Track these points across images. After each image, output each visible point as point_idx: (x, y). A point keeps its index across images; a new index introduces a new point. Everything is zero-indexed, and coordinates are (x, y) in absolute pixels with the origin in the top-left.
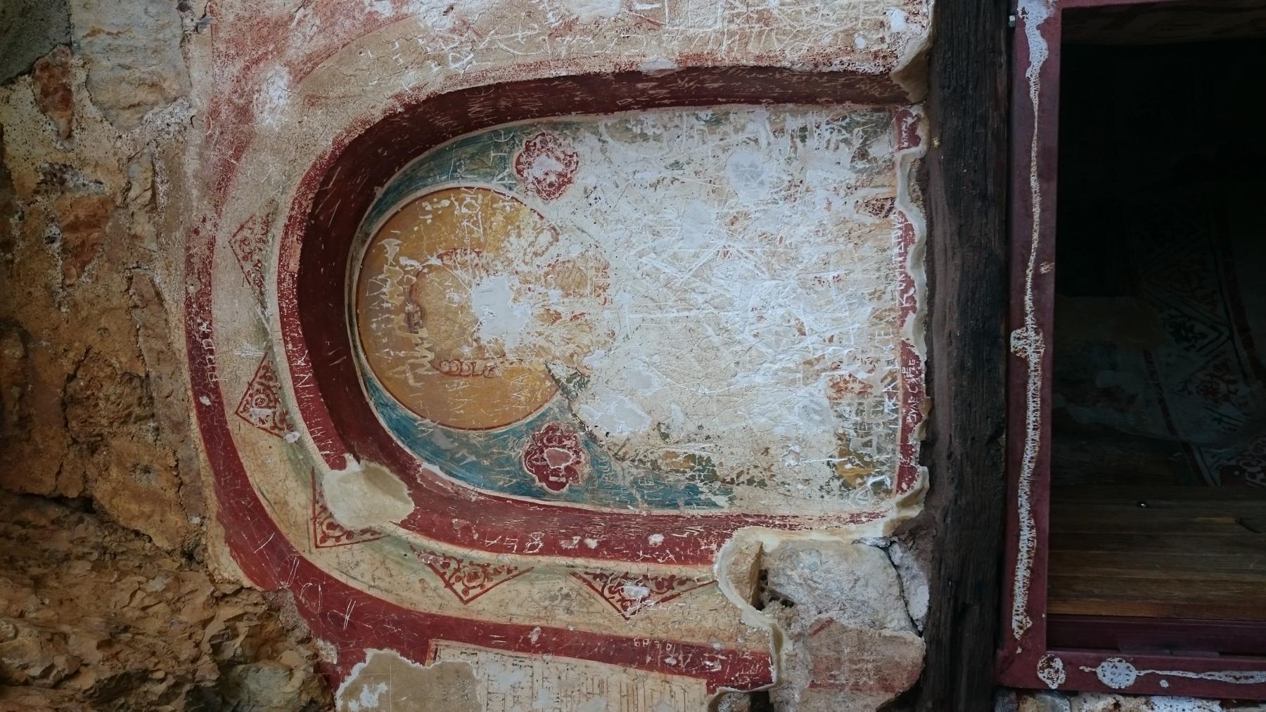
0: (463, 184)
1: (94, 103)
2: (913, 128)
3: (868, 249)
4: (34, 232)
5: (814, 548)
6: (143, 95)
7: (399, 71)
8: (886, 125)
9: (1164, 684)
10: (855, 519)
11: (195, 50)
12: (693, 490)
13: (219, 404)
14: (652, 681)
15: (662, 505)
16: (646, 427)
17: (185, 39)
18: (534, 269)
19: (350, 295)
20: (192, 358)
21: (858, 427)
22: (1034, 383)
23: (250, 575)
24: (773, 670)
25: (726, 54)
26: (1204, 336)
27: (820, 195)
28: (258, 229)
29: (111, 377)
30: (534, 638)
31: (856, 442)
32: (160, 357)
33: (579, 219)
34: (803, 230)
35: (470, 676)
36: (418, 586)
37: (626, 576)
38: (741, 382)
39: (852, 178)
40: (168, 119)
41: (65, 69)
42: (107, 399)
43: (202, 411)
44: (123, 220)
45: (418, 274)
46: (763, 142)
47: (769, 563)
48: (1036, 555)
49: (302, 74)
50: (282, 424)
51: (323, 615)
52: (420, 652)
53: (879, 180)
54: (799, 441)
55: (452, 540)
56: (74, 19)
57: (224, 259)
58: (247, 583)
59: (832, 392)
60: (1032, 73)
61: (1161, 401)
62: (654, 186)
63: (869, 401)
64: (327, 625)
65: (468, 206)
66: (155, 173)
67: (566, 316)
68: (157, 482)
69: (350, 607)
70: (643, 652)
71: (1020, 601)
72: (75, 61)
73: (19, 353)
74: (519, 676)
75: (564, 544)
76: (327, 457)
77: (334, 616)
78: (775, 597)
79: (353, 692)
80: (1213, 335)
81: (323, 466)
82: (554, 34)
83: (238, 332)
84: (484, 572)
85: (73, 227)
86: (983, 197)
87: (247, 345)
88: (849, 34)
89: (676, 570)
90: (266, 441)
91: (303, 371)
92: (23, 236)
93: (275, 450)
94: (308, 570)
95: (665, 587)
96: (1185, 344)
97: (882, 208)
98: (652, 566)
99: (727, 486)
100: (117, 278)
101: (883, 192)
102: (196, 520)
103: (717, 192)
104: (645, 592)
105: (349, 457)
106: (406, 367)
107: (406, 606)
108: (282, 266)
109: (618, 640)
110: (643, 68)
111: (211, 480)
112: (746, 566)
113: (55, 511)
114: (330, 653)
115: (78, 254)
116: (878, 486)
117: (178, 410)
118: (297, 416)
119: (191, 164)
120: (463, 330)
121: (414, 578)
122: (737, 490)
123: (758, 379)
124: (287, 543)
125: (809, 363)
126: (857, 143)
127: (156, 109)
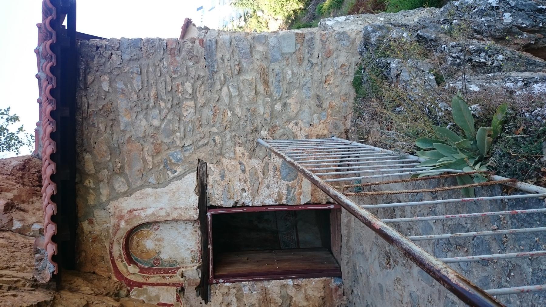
3: (194, 236)
5: (188, 270)
6: (104, 223)
7: (139, 221)
11: (111, 218)
12: (174, 265)
13: (114, 259)
14: (169, 288)
16: (168, 257)
17: (110, 217)
22: (211, 251)
27: (189, 230)
31: (194, 257)
32: (105, 254)
41: (92, 219)
43: (112, 260)
47: (183, 273)
48: (212, 269)
49: (126, 221)
50: (122, 261)
57: (115, 243)
60: (209, 220)
64: (129, 285)
71: (210, 274)
73: (85, 254)
74: (154, 289)
79: (132, 293)
84: (149, 277)
90: (120, 263)
94: (126, 278)
95: (171, 277)
97: (196, 231)
99: (179, 264)
103: (177, 230)
113: (89, 274)
114: (129, 288)
115: (93, 242)
118: (124, 260)
119: (111, 231)
123: (182, 251)
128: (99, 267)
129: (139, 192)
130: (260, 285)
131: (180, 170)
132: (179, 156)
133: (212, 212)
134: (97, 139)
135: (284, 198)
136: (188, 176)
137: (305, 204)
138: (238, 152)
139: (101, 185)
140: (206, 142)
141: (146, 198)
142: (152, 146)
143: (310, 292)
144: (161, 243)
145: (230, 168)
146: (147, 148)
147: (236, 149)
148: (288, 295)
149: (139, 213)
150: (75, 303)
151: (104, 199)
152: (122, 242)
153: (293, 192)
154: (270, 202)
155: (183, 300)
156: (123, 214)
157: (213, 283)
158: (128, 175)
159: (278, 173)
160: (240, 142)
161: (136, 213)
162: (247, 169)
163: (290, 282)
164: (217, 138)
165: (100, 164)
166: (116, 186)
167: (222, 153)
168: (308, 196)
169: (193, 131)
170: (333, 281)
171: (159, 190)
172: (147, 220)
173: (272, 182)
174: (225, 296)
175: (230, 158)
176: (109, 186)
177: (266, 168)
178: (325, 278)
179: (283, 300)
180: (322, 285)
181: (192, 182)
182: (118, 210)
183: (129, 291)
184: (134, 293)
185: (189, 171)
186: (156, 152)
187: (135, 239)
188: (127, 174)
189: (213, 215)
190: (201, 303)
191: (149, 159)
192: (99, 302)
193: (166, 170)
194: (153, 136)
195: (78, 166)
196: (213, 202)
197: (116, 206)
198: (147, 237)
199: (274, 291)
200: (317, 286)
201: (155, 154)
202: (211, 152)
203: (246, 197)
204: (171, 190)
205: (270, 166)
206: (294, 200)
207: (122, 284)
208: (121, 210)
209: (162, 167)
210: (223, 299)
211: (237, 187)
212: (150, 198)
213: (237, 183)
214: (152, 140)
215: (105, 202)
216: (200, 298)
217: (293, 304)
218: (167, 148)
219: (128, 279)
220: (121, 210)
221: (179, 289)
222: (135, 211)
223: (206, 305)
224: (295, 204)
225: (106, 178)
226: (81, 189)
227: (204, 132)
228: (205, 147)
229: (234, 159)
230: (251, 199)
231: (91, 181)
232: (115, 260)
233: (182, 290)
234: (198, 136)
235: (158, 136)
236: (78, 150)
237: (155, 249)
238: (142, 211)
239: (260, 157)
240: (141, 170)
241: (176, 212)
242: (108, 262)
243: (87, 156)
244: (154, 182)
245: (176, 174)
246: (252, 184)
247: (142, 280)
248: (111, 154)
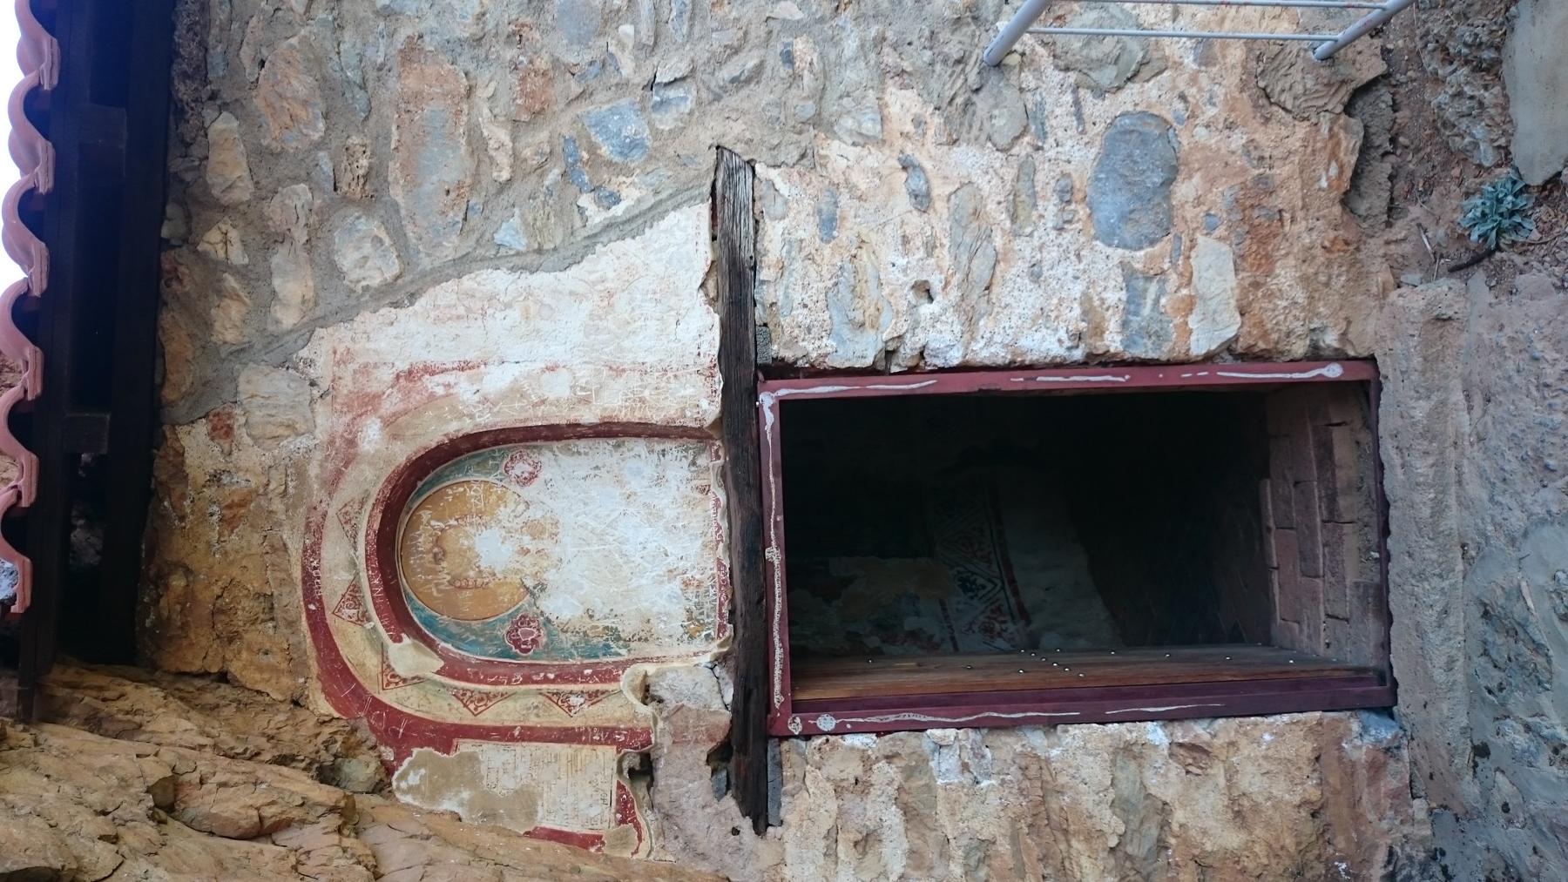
0: (472, 479)
1: (249, 435)
2: (717, 451)
3: (698, 510)
4: (200, 510)
5: (675, 670)
6: (281, 431)
7: (447, 422)
8: (704, 450)
9: (849, 726)
10: (696, 654)
11: (319, 407)
12: (607, 647)
13: (322, 609)
14: (586, 750)
15: (589, 657)
16: (580, 612)
17: (312, 401)
18: (514, 525)
19: (398, 545)
20: (304, 582)
21: (697, 604)
23: (338, 710)
24: (652, 736)
25: (623, 416)
26: (984, 587)
27: (673, 483)
28: (356, 506)
29: (247, 596)
30: (517, 733)
31: (696, 613)
32: (282, 582)
33: (542, 497)
34: (666, 501)
35: (477, 759)
36: (447, 708)
37: (571, 693)
38: (634, 583)
39: (689, 475)
40: (298, 445)
41: (230, 416)
42: (244, 609)
43: (309, 614)
44: (263, 502)
45: (442, 530)
46: (643, 456)
47: (649, 681)
48: (783, 662)
49: (389, 423)
50: (364, 618)
51: (386, 731)
52: (446, 747)
53: (702, 476)
54: (666, 614)
55: (468, 680)
56: (240, 389)
58: (336, 715)
59: (683, 586)
60: (768, 428)
61: (953, 639)
62: (585, 479)
63: (702, 590)
65: (475, 491)
66: (287, 475)
67: (533, 550)
68: (275, 659)
69: (403, 724)
70: (580, 734)
71: (777, 688)
72: (238, 411)
73: (183, 583)
74: (508, 756)
75: (535, 678)
76: (391, 636)
77: (393, 731)
78: (653, 699)
79: (403, 776)
80: (990, 586)
81: (389, 641)
82: (534, 405)
83: (337, 565)
84: (488, 697)
85: (229, 507)
86: (748, 485)
87: (342, 573)
88: (683, 409)
89: (600, 687)
91: (377, 586)
92: (193, 512)
93: (358, 634)
94: (378, 704)
95: (593, 697)
96: (970, 594)
97: (704, 490)
98: (586, 686)
100: (256, 536)
101: (705, 482)
102: (302, 680)
103: (619, 482)
104: (582, 700)
105: (404, 635)
106: (432, 586)
107: (439, 720)
108: (369, 527)
109: (566, 729)
110: (582, 422)
111: (314, 654)
112: (638, 681)
113: (199, 683)
114: (389, 754)
115: (229, 523)
116: (707, 636)
117: (293, 614)
119: (313, 470)
120: (470, 561)
121: (444, 704)
122: (632, 645)
123: (644, 581)
124: (364, 689)
125: (671, 571)
126: (691, 458)
127: (290, 439)
128: (249, 649)
129: (451, 285)
130: (1011, 745)
131: (635, 194)
132: (629, 130)
133: (783, 392)
134: (271, 45)
135: (1113, 324)
136: (672, 217)
137: (1209, 358)
138: (894, 110)
139: (279, 258)
140: (751, 64)
141: (484, 315)
142: (513, 79)
143: (1252, 782)
144: (546, 544)
145: (863, 186)
146: (490, 90)
147: (887, 97)
148: (1148, 796)
149: (448, 386)
150: (106, 770)
151: (288, 318)
152: (367, 522)
153: (1151, 295)
154: (1046, 344)
155: (646, 818)
156: (374, 388)
157: (790, 736)
158: (403, 212)
159: (1083, 212)
160: (906, 65)
161: (434, 384)
162: (935, 193)
163: (1155, 733)
164: (800, 46)
165: (277, 155)
166: (347, 259)
167: (825, 115)
168: (1226, 316)
169: (692, 18)
170: (1355, 727)
171: (541, 279)
172: (486, 420)
173: (1053, 254)
174: (848, 796)
175: (862, 140)
176: (312, 261)
177: (1023, 186)
178: (1318, 714)
179: (1126, 822)
180: (1308, 749)
181: (691, 247)
182: (352, 367)
183: (389, 770)
184: (413, 779)
185: (678, 198)
186: (528, 109)
187: (427, 525)
188: (396, 207)
189: (784, 406)
190: (735, 832)
191: (499, 135)
192: (237, 778)
193: (574, 189)
194: (516, 37)
195: (176, 164)
196: (786, 346)
197: (341, 349)
198: (483, 515)
199: (1084, 773)
200: (1284, 753)
201: (525, 117)
202: (775, 112)
203: (935, 319)
204: (594, 284)
205: (1040, 177)
206: (1159, 337)
207: (354, 730)
208: (365, 370)
209: (553, 175)
210: (841, 812)
211: (894, 276)
212: (499, 315)
213: (890, 254)
214: (510, 54)
215: (290, 332)
216: (730, 803)
217: (1173, 841)
218: (576, 89)
219: (384, 706)
220: (365, 370)
221: (633, 761)
222: (433, 373)
223: (760, 844)
224: (1162, 354)
225: (303, 221)
226: (182, 269)
227: (744, 21)
228: (744, 92)
229: (882, 142)
230: (957, 328)
231: (234, 235)
232: (328, 614)
233: (644, 770)
234: (719, 40)
235: (537, 35)
236: (183, 91)
237: (517, 572)
238: (463, 375)
239: (996, 137)
240: (460, 185)
241: (619, 384)
242: (292, 624)
243: (223, 125)
244: (521, 243)
245: (618, 210)
246: (964, 259)
247: (453, 712)
248: (326, 116)
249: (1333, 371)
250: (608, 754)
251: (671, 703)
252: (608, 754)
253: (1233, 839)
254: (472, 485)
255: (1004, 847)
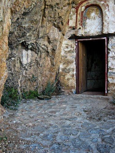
14: (75, 23)
49: (103, 4)
95: (79, 24)
130: (74, 60)
135: (111, 71)
137: (108, 80)
143: (71, 80)
144: (93, 19)
154: (110, 65)
155: (70, 29)
161: (107, 7)
163: (75, 73)
172: (104, 12)
187: (95, 9)
189: (104, 40)
198: (96, 14)
216: (71, 36)
221: (74, 28)
224: (108, 76)
233: (74, 29)
247: (78, 12)
249: (106, 92)
250: (75, 25)
251: (79, 31)
252: (75, 25)
253: (66, 78)
254: (99, 12)
255: (66, 59)
